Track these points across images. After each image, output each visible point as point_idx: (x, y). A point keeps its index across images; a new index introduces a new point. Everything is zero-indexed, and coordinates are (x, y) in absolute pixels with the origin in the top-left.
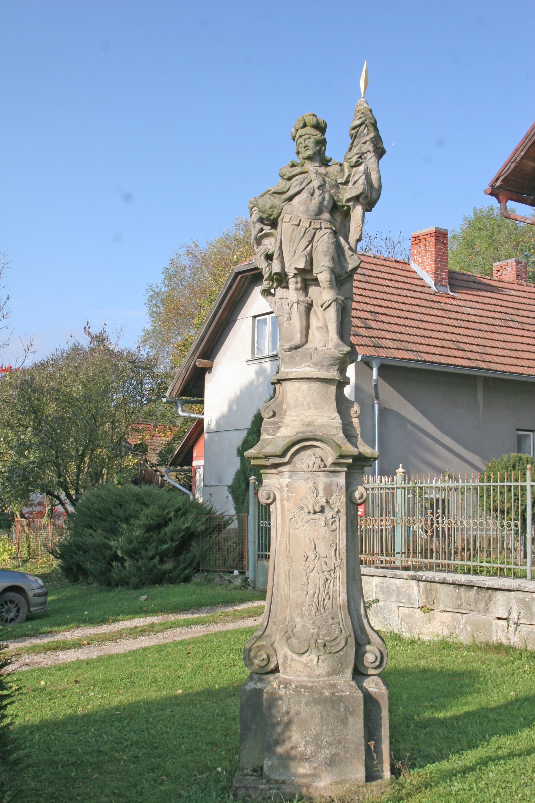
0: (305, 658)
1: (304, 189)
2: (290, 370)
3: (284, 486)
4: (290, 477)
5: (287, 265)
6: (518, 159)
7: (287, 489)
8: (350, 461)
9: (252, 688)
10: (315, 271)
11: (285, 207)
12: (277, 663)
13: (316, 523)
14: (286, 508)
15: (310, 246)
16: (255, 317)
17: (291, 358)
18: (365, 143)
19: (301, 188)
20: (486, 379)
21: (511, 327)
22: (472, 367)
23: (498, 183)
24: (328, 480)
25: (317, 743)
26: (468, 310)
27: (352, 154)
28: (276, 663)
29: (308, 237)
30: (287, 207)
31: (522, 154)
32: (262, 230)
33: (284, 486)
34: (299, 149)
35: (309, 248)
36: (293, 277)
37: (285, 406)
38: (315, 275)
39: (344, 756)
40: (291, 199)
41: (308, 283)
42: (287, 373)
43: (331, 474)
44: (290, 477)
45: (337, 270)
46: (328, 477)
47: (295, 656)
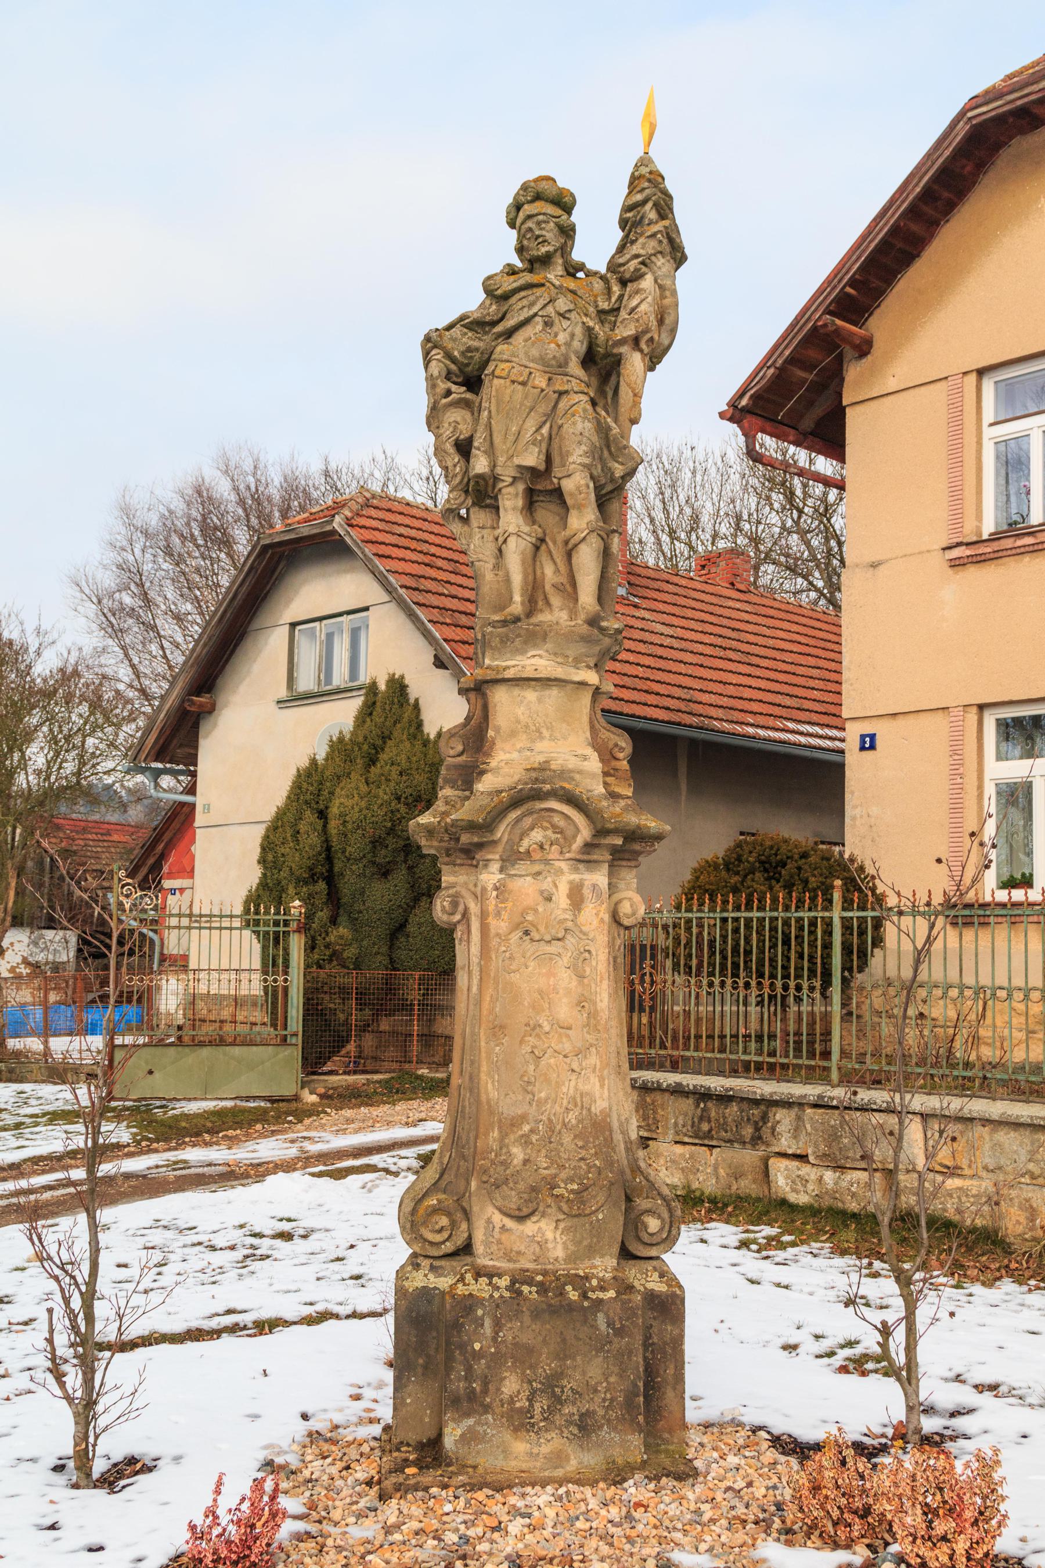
0: (530, 1228)
1: (536, 315)
2: (504, 664)
3: (490, 887)
4: (501, 871)
5: (501, 460)
6: (780, 362)
7: (495, 893)
8: (619, 841)
9: (420, 1285)
10: (557, 472)
11: (499, 348)
12: (470, 1237)
13: (551, 959)
14: (493, 931)
15: (548, 425)
16: (293, 625)
17: (504, 640)
18: (653, 235)
19: (531, 313)
20: (693, 742)
21: (730, 660)
22: (673, 723)
23: (744, 402)
24: (576, 877)
25: (553, 1392)
26: (659, 628)
27: (628, 256)
28: (466, 1235)
29: (543, 408)
30: (502, 349)
31: (787, 353)
32: (449, 393)
33: (490, 887)
34: (525, 242)
35: (545, 431)
36: (512, 484)
37: (491, 733)
38: (555, 481)
39: (604, 1417)
40: (509, 334)
41: (535, 498)
42: (497, 669)
43: (581, 866)
44: (501, 870)
45: (597, 471)
46: (576, 870)
47: (509, 1223)
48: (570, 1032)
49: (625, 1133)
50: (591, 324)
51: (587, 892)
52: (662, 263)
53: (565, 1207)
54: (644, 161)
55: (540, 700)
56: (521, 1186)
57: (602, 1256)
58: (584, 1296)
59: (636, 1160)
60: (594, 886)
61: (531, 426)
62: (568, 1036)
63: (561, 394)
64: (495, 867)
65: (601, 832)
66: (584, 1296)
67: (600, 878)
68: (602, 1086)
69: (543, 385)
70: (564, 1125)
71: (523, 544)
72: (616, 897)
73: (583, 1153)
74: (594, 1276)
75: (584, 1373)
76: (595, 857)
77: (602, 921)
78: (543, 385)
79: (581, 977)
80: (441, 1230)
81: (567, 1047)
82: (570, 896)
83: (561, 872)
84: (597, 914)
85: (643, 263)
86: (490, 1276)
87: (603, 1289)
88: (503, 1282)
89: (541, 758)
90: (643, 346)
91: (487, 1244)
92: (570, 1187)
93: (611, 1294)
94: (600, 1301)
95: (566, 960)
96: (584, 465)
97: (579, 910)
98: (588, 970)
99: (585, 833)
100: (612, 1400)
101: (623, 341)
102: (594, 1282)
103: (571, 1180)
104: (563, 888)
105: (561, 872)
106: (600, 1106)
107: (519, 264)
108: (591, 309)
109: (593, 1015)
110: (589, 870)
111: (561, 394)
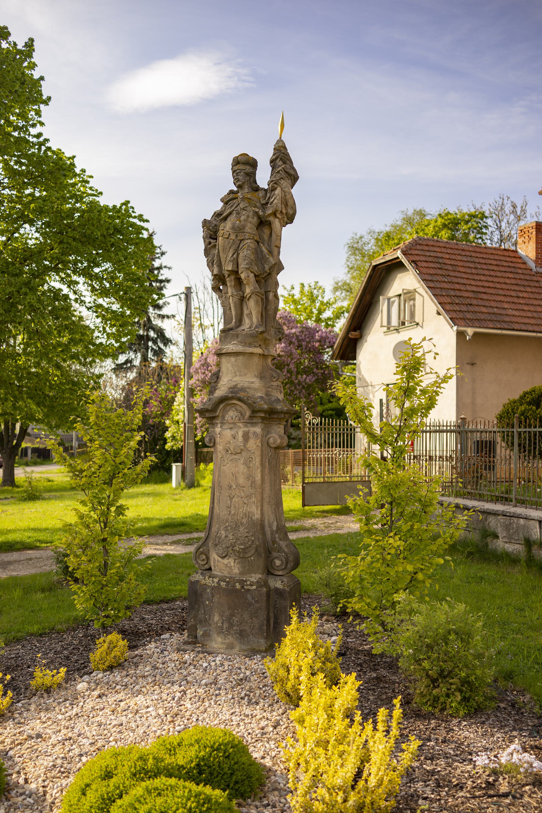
0: (226, 561)
24: (246, 429)
43: (248, 425)
46: (246, 426)
47: (220, 559)
48: (244, 489)
49: (270, 526)
50: (257, 210)
51: (251, 435)
52: (285, 183)
53: (237, 554)
54: (280, 140)
55: (236, 361)
56: (224, 546)
57: (255, 573)
58: (243, 587)
59: (275, 538)
60: (254, 432)
61: (230, 255)
62: (243, 490)
63: (241, 240)
64: (219, 425)
65: (254, 412)
66: (243, 587)
67: (258, 429)
68: (257, 509)
69: (234, 238)
70: (241, 524)
71: (235, 299)
72: (268, 436)
73: (247, 534)
74: (249, 580)
75: (242, 616)
76: (254, 421)
77: (258, 446)
78: (234, 238)
79: (249, 468)
80: (203, 560)
81: (243, 494)
82: (243, 437)
83: (240, 427)
84: (255, 443)
85: (275, 183)
86: (213, 578)
87: (251, 585)
88: (216, 580)
89: (234, 384)
90: (278, 216)
91: (215, 567)
92: (241, 547)
93: (254, 587)
94: (249, 590)
95: (242, 461)
96: (247, 268)
97: (247, 442)
98: (251, 465)
99: (248, 413)
100: (254, 626)
101: (270, 215)
102: (248, 583)
103: (242, 544)
104: (240, 433)
105: (240, 427)
106: (126, 512)
107: (235, 189)
108: (258, 204)
109: (254, 482)
110: (252, 426)
111: (241, 240)
